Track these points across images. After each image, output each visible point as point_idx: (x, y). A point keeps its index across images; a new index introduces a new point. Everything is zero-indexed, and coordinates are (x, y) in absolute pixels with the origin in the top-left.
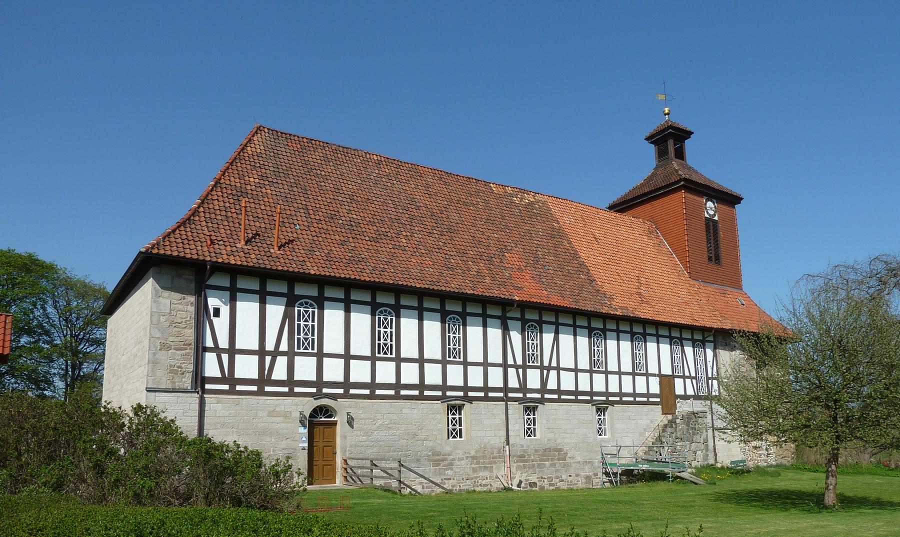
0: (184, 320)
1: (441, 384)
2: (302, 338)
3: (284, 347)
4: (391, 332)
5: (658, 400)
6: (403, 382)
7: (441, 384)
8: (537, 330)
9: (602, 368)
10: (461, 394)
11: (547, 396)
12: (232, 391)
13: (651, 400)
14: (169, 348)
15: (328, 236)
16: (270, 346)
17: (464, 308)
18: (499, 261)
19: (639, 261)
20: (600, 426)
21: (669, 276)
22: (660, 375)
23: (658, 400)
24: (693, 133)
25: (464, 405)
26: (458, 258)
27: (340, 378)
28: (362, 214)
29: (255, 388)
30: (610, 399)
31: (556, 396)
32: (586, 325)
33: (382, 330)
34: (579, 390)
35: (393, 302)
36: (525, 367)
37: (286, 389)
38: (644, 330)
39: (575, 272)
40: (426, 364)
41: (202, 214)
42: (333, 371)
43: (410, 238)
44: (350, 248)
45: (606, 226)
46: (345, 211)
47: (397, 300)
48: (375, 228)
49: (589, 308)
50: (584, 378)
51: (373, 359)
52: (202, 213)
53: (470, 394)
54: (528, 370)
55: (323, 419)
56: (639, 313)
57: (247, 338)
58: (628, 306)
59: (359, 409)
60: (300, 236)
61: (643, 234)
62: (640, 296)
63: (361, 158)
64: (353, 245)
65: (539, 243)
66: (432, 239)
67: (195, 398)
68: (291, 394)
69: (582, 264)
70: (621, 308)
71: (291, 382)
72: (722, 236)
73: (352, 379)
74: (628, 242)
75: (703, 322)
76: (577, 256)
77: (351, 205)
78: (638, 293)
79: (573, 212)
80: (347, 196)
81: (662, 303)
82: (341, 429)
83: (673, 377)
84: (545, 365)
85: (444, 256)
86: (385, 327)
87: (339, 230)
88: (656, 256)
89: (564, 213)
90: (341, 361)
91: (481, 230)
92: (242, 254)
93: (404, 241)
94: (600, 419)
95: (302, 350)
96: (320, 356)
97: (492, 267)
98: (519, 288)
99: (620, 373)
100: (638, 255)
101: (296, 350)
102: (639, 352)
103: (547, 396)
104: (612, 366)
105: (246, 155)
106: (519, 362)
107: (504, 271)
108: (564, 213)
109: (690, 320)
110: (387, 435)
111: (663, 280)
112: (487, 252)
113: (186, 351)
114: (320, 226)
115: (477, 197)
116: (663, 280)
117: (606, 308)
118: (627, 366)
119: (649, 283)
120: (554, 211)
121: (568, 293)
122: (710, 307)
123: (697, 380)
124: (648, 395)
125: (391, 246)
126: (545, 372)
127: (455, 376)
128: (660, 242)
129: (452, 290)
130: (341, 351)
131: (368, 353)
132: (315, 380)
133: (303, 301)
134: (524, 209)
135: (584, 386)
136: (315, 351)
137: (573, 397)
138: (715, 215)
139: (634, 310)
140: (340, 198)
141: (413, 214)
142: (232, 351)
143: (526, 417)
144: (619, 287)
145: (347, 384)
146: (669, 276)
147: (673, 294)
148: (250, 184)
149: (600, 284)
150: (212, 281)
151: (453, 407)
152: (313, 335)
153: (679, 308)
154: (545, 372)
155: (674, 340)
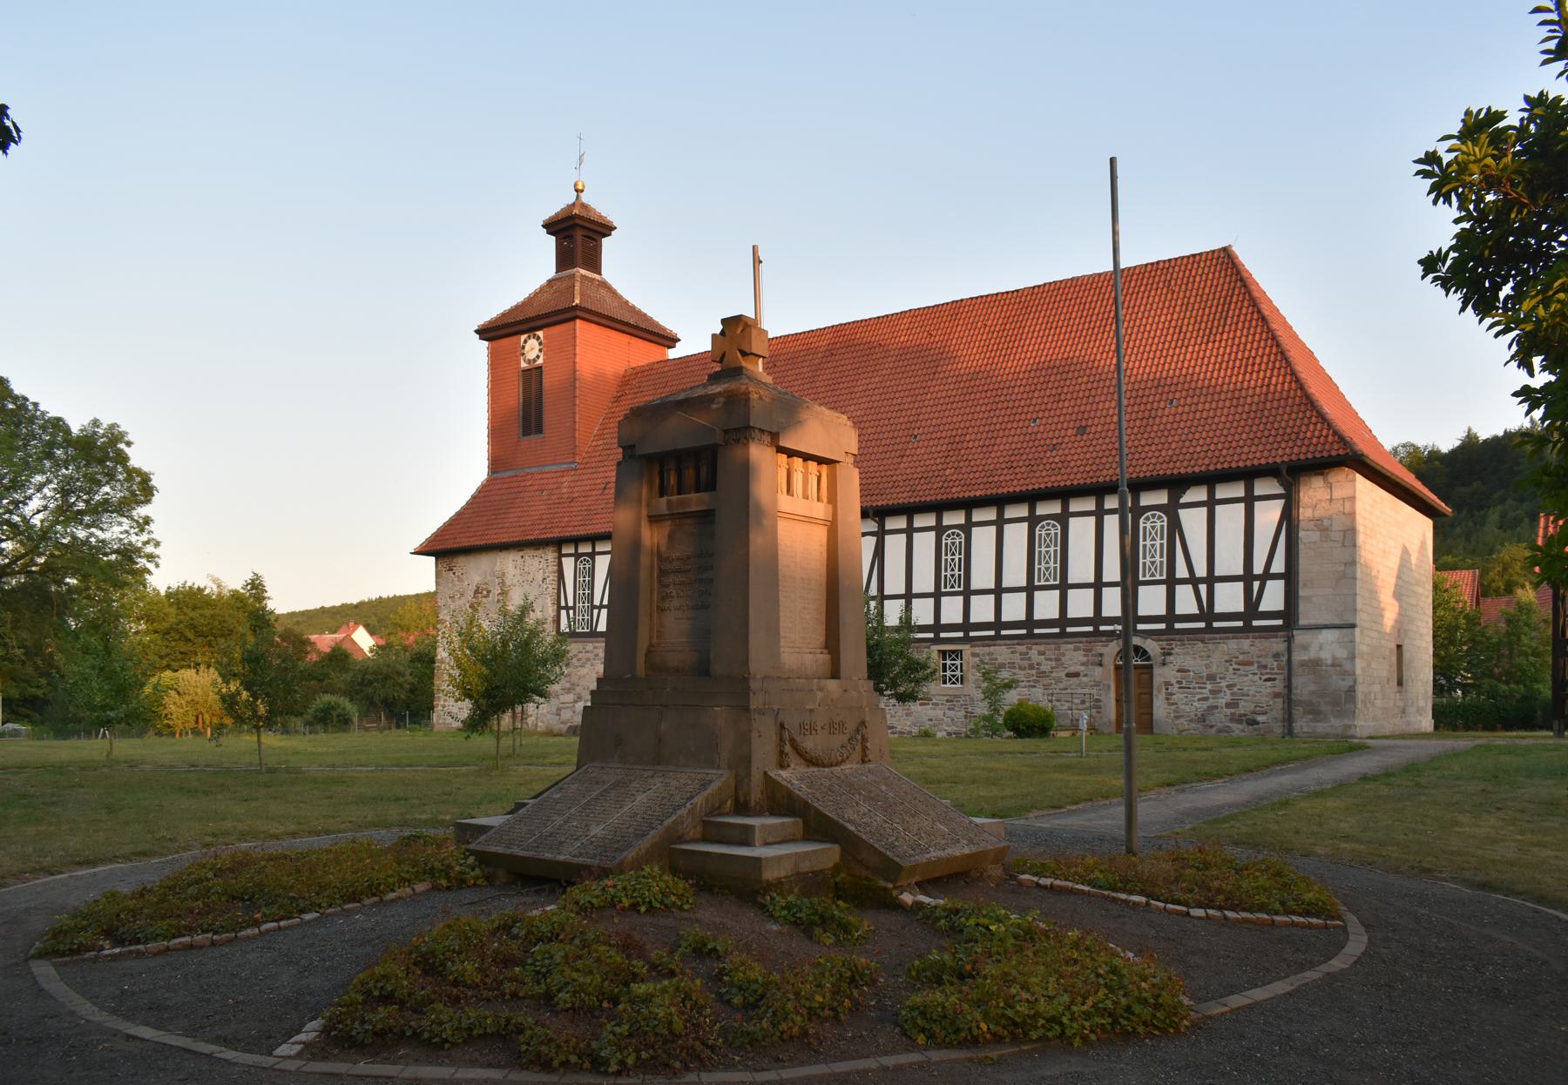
4: (946, 555)
5: (1280, 622)
16: (1258, 569)
23: (1280, 622)
29: (1240, 624)
42: (982, 610)
57: (1230, 560)
59: (1187, 658)
82: (1156, 671)
127: (923, 612)
132: (1035, 618)
142: (1211, 579)
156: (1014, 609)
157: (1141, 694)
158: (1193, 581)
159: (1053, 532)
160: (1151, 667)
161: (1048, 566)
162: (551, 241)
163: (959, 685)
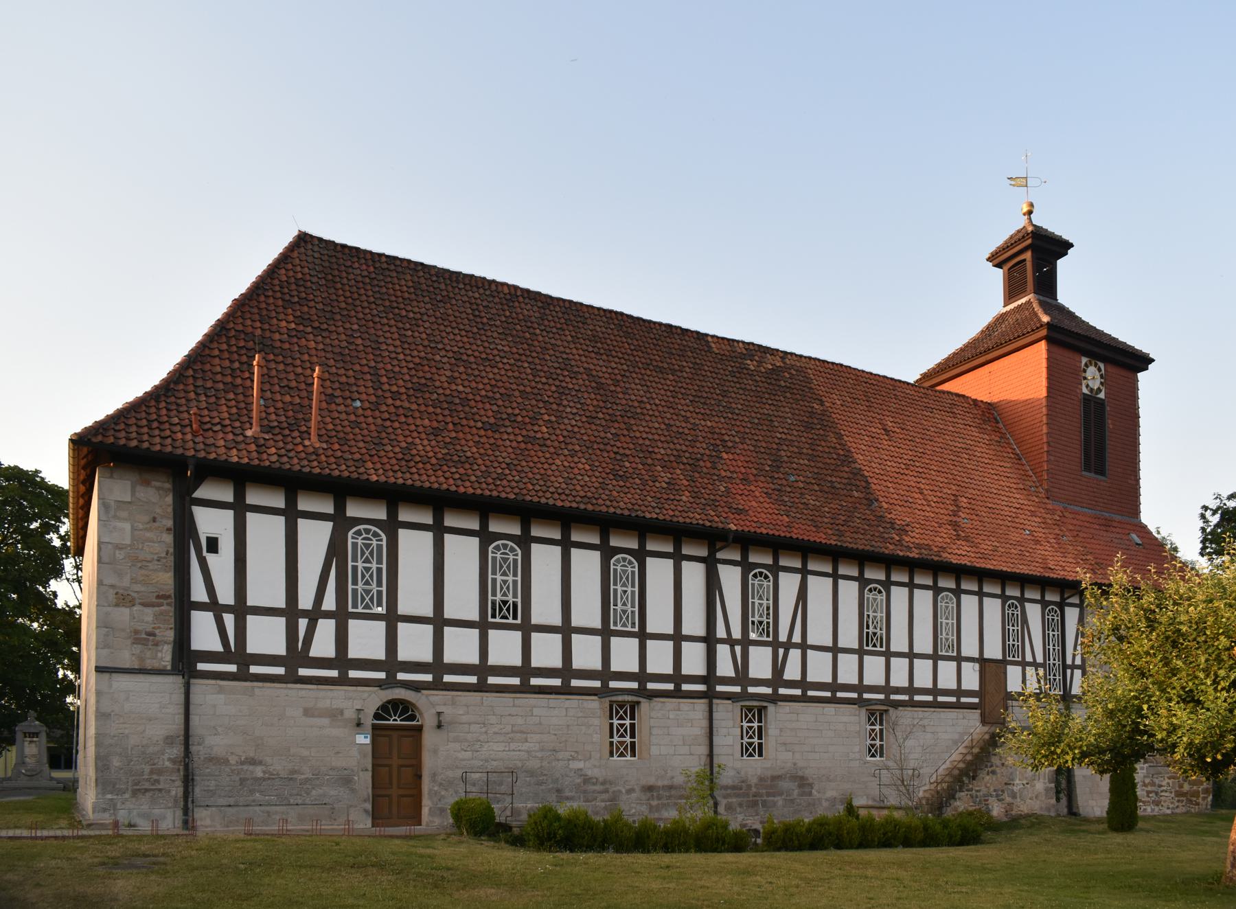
0: (156, 557)
1: (600, 669)
2: (360, 590)
3: (329, 603)
5: (976, 700)
6: (535, 663)
7: (600, 669)
8: (634, 567)
9: (881, 647)
10: (634, 685)
11: (782, 691)
12: (242, 676)
13: (963, 700)
14: (132, 603)
15: (410, 421)
16: (306, 601)
17: (776, 560)
18: (709, 465)
19: (960, 469)
20: (873, 742)
21: (1011, 495)
22: (982, 661)
23: (976, 700)
24: (1071, 245)
25: (638, 703)
26: (638, 460)
27: (427, 656)
28: (473, 385)
29: (280, 671)
30: (893, 697)
31: (798, 692)
32: (1038, 597)
33: (499, 578)
34: (839, 682)
35: (953, 586)
36: (746, 643)
37: (334, 673)
38: (958, 584)
39: (843, 486)
40: (574, 636)
41: (191, 380)
43: (556, 426)
44: (448, 440)
45: (906, 409)
46: (444, 379)
47: (526, 528)
48: (495, 408)
49: (860, 545)
50: (923, 669)
51: (483, 626)
52: (191, 378)
53: (650, 686)
54: (752, 649)
55: (399, 722)
56: (949, 556)
58: (931, 543)
60: (362, 419)
61: (971, 424)
62: (956, 527)
63: (481, 291)
64: (454, 435)
65: (784, 436)
66: (594, 427)
67: (175, 682)
68: (343, 681)
69: (857, 473)
70: (919, 546)
71: (342, 660)
72: (1111, 426)
73: (402, 656)
74: (944, 437)
75: (1062, 573)
76: (851, 460)
77: (456, 369)
78: (951, 523)
79: (850, 386)
80: (450, 354)
81: (993, 539)
82: (429, 738)
83: (1004, 663)
84: (1038, 661)
85: (613, 455)
86: (504, 574)
87: (431, 409)
88: (990, 462)
89: (834, 387)
90: (429, 629)
91: (683, 413)
92: (253, 447)
93: (545, 429)
94: (873, 730)
95: (360, 610)
96: (392, 619)
97: (697, 475)
98: (739, 512)
99: (911, 655)
100: (958, 459)
101: (350, 610)
102: (947, 621)
103: (782, 691)
104: (899, 643)
105: (276, 282)
106: (737, 634)
107: (717, 482)
108: (834, 387)
109: (1039, 569)
110: (507, 749)
111: (999, 502)
112: (691, 450)
113: (162, 608)
114: (398, 403)
115: (682, 359)
116: (999, 502)
117: (891, 547)
118: (924, 644)
119: (974, 507)
120: (816, 383)
121: (826, 520)
122: (1079, 548)
123: (1045, 670)
124: (959, 692)
125: (520, 439)
126: (781, 651)
127: (624, 655)
128: (1001, 438)
129: (783, 535)
130: (428, 611)
131: (474, 616)
133: (361, 527)
134: (764, 380)
135: (847, 674)
136: (519, 621)
137: (828, 694)
138: (1099, 390)
139: (941, 550)
140: (438, 358)
141: (564, 384)
142: (242, 609)
143: (745, 725)
144: (919, 513)
145: (438, 666)
146: (1011, 495)
147: (1014, 525)
148: (278, 331)
149: (885, 506)
150: (202, 493)
151: (621, 705)
152: (379, 584)
153: (1023, 549)
154: (781, 651)
155: (1010, 602)
156: (587, 653)
157: (402, 766)
158: (213, 605)
159: (511, 557)
160: (419, 729)
161: (624, 605)
162: (999, 274)
163: (878, 758)
